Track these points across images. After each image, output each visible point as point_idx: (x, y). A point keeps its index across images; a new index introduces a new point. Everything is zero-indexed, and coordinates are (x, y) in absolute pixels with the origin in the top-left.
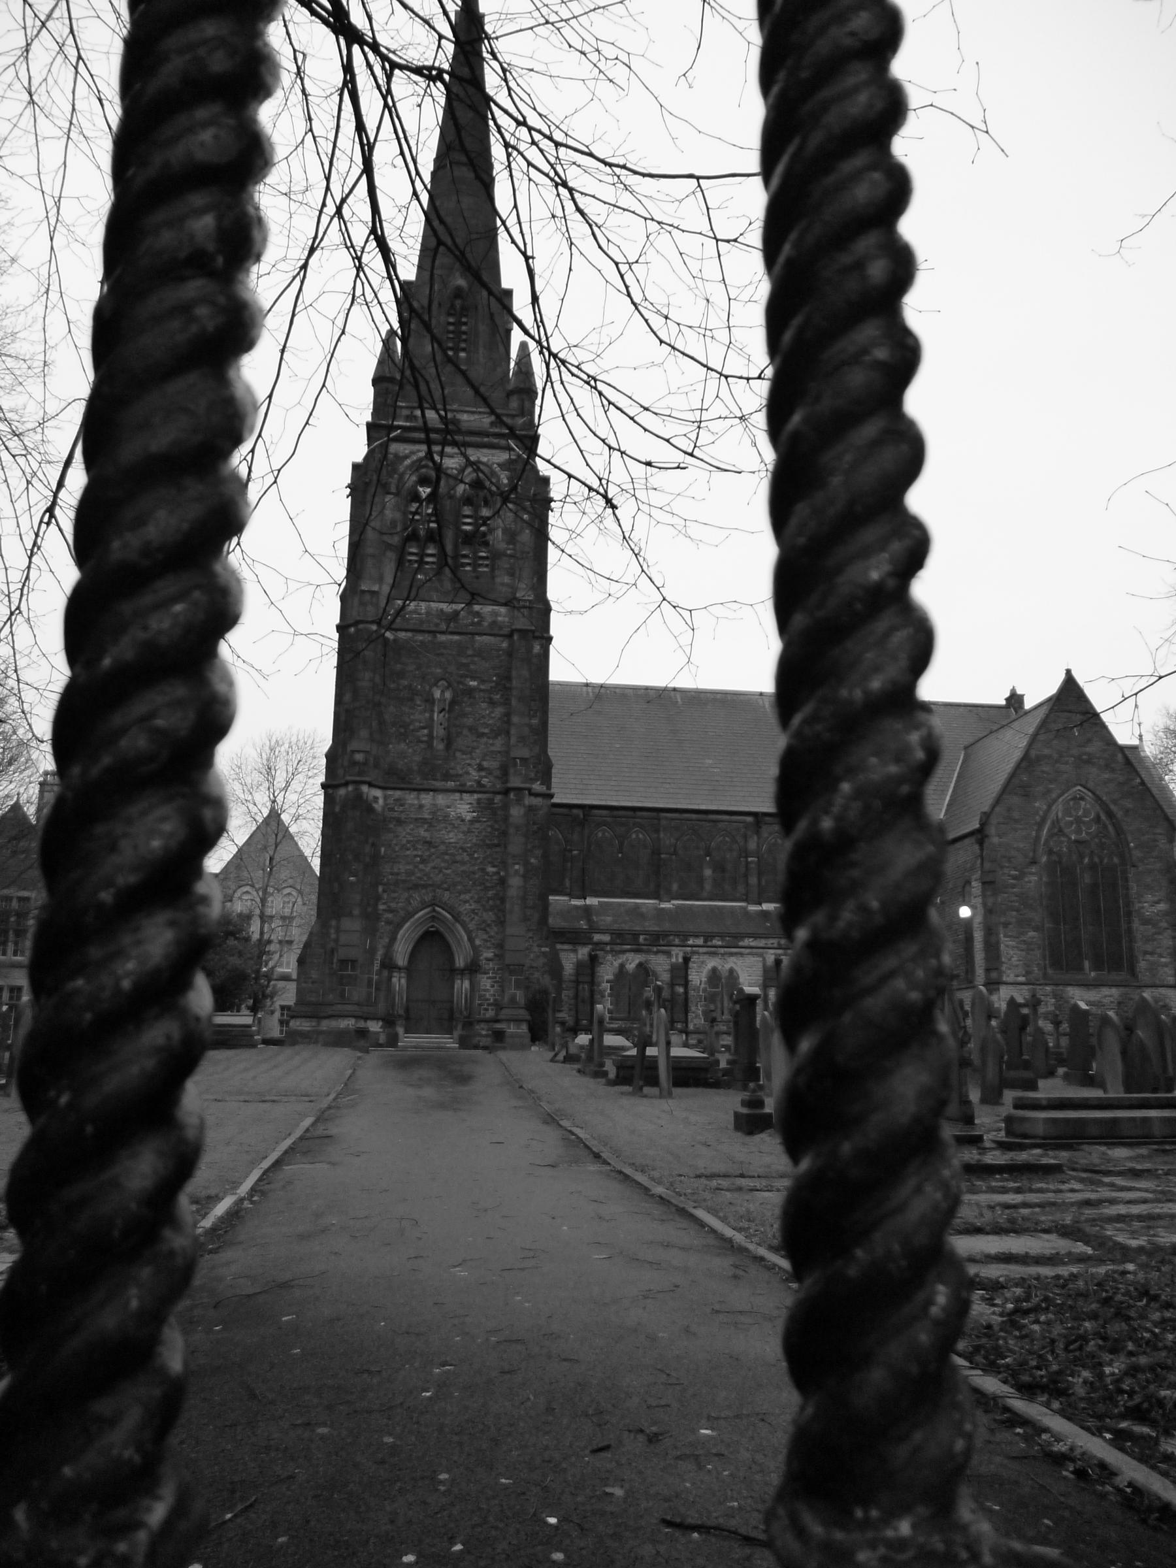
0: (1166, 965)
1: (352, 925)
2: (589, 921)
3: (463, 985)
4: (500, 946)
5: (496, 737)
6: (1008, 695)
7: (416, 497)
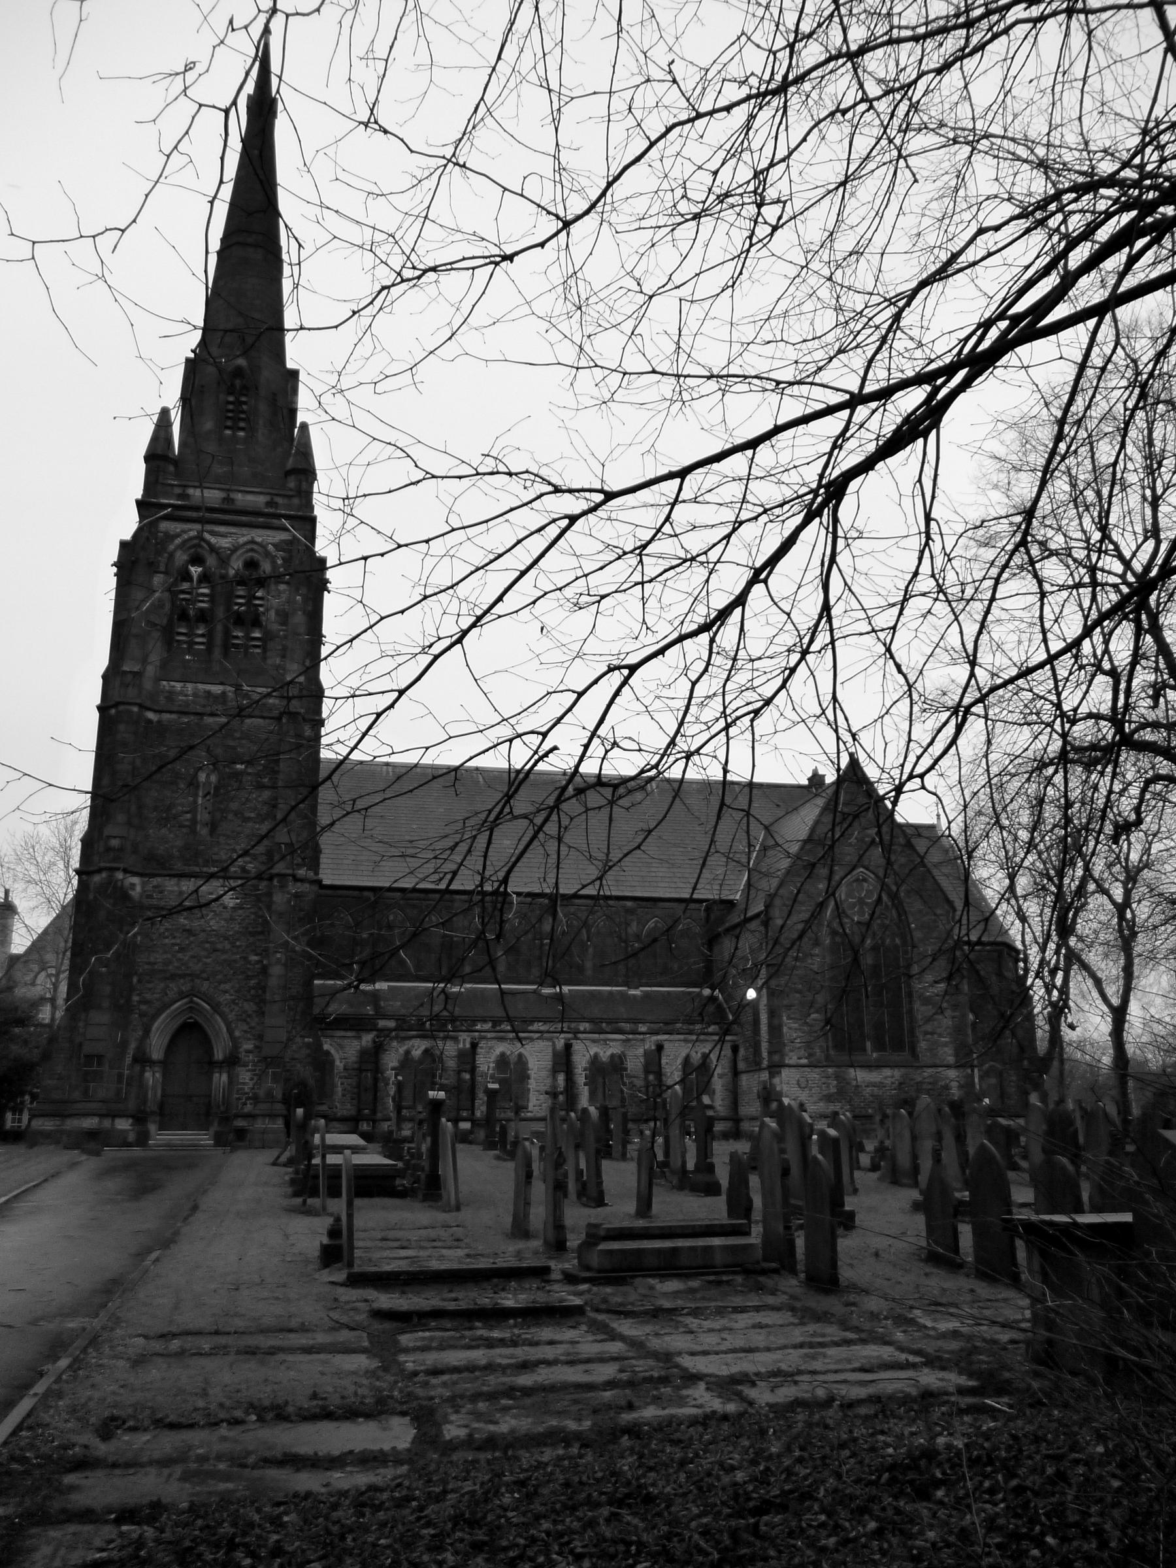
0: (945, 1044)
1: (100, 1019)
2: (377, 1007)
3: (221, 1079)
4: (260, 1037)
5: (262, 822)
6: (810, 775)
7: (187, 577)
